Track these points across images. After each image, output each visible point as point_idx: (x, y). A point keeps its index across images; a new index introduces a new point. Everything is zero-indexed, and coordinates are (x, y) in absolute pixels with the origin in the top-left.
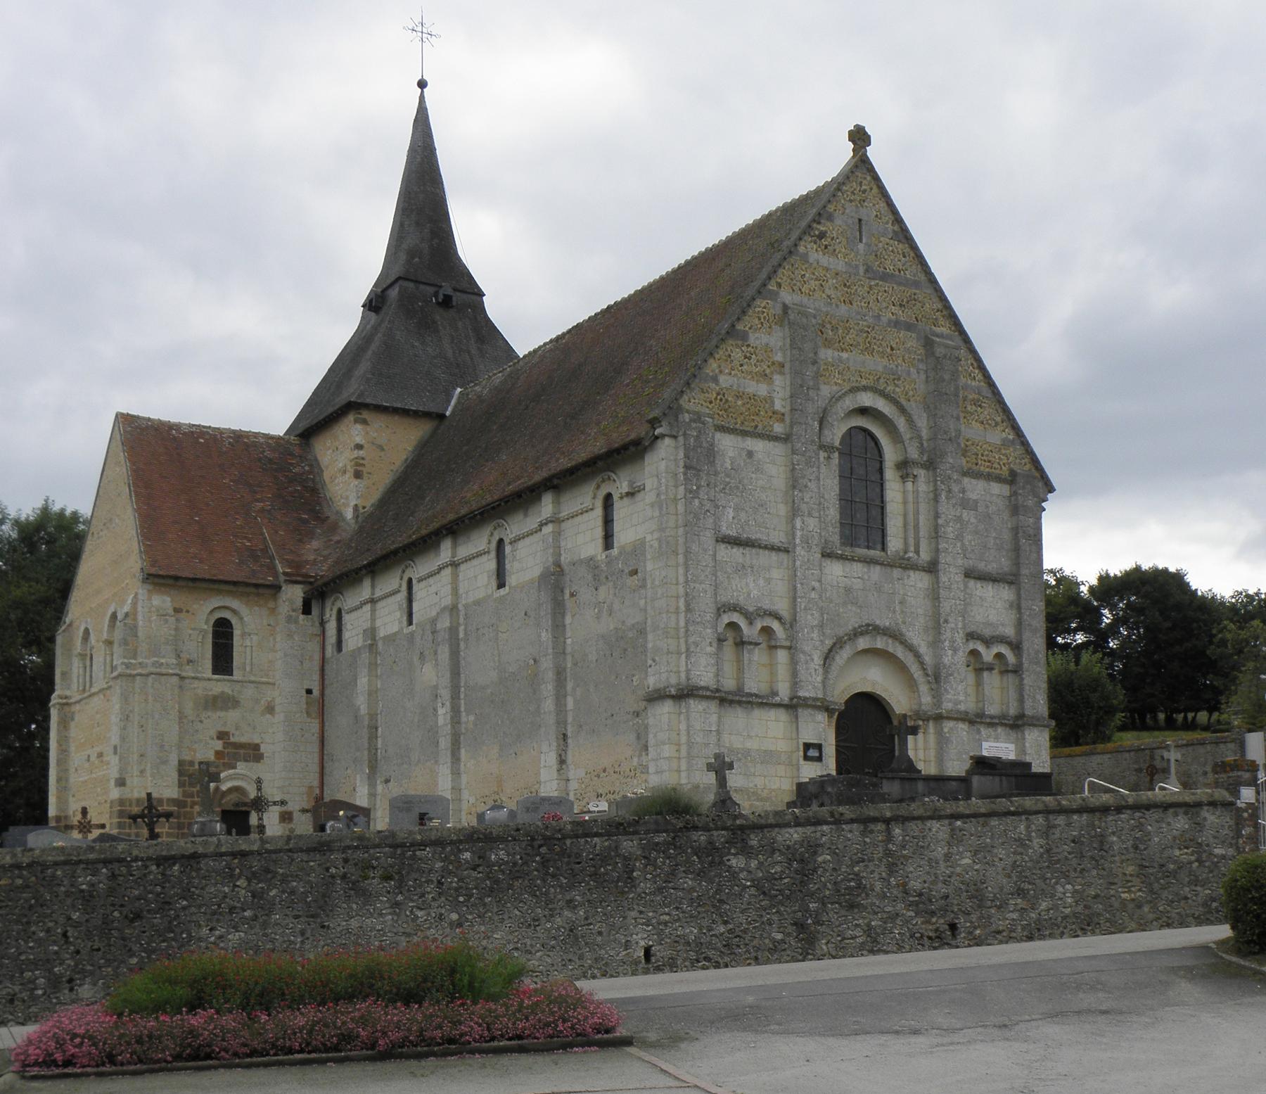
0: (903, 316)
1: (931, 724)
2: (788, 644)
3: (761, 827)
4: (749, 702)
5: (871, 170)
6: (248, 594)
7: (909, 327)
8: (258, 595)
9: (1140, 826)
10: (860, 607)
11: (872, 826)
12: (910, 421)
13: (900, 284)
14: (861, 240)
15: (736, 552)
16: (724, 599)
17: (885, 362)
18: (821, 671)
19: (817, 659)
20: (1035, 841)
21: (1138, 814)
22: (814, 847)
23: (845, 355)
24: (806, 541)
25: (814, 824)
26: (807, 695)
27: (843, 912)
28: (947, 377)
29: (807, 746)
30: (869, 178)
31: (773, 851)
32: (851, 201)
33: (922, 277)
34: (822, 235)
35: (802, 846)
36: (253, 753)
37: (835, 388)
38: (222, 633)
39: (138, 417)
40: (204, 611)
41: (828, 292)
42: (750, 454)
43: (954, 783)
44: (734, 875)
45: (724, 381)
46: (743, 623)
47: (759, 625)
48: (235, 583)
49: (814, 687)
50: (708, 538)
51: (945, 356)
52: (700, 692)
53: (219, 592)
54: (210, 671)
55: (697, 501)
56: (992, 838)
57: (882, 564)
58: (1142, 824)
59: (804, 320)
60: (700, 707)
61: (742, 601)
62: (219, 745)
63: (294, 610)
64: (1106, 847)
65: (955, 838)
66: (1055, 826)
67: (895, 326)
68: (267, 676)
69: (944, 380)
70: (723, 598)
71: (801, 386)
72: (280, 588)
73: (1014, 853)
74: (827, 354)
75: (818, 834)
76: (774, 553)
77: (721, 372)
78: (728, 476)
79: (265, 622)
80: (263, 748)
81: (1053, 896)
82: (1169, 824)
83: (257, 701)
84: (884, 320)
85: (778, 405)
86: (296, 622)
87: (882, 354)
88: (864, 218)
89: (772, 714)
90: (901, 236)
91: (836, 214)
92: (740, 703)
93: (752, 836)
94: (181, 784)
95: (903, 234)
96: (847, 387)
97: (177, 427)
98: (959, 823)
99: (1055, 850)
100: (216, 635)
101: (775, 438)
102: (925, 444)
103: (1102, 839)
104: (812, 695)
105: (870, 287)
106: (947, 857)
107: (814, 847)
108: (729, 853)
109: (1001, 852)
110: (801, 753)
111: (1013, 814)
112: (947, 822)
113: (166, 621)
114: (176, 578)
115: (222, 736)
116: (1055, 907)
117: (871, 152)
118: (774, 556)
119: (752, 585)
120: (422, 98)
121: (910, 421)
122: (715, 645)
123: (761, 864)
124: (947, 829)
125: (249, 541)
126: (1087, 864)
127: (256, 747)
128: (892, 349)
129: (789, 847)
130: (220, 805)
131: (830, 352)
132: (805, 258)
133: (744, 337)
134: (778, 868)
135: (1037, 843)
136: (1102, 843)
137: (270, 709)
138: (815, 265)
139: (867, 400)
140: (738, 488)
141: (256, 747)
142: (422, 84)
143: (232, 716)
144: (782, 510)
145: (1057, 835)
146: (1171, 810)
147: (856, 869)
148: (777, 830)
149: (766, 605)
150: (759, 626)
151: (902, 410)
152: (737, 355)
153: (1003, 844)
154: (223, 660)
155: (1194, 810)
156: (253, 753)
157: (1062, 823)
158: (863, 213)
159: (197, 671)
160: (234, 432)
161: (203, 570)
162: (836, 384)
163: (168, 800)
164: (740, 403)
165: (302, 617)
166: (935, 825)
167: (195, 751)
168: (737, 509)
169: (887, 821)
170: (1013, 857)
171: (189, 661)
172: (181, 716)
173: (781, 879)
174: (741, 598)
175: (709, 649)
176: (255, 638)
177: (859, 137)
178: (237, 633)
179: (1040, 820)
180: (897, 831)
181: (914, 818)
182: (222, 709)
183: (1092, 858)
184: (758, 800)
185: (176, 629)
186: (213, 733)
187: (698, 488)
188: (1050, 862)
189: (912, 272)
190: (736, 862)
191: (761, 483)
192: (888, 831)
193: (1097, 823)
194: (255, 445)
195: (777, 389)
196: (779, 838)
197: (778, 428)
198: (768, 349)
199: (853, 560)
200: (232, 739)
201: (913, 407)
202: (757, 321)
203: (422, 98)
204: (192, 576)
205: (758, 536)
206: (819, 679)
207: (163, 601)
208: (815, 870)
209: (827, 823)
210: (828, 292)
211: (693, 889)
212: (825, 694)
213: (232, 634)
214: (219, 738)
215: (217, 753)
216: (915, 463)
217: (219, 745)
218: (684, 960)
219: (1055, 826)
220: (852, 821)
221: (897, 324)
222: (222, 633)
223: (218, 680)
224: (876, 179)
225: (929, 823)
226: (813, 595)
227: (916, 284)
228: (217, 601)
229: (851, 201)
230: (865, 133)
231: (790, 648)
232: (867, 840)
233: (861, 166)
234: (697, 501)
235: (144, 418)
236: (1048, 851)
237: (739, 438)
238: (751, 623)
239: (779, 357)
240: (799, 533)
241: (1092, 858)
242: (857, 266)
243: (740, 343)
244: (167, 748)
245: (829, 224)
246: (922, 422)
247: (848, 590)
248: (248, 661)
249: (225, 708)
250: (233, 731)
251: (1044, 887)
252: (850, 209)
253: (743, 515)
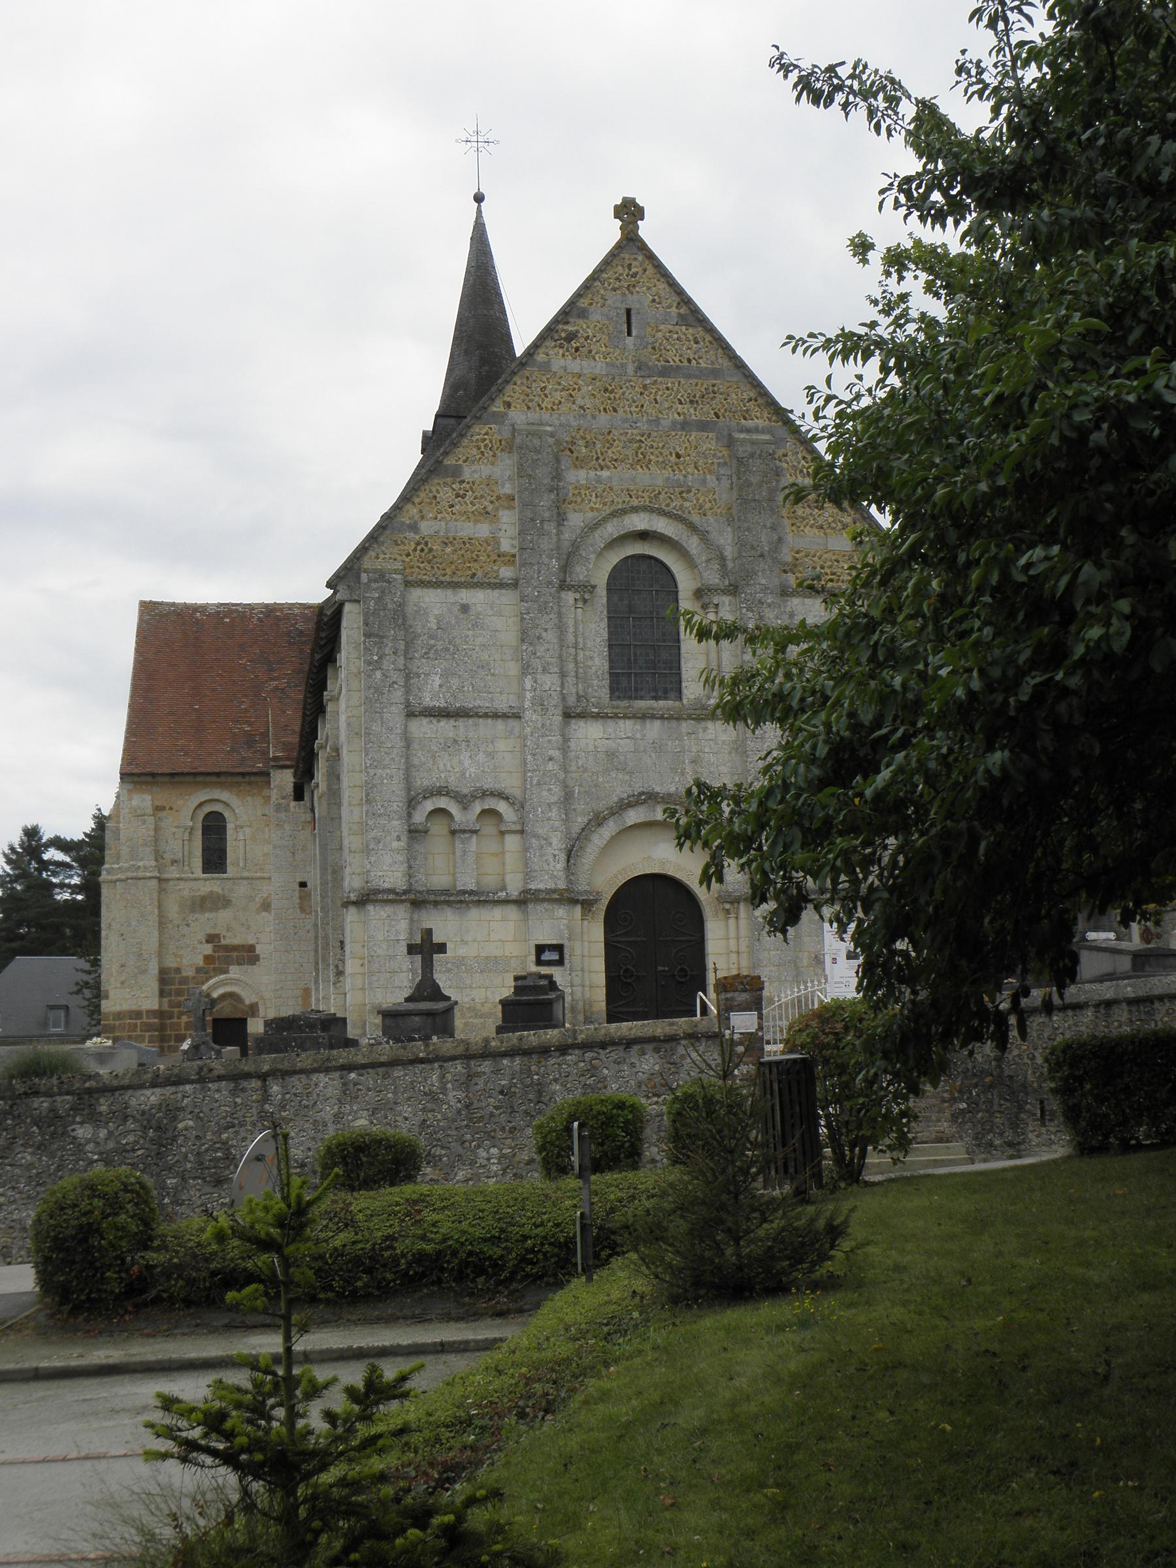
0: (694, 415)
1: (742, 906)
2: (518, 828)
3: (112, 1090)
4: (461, 902)
5: (643, 247)
6: (239, 784)
7: (703, 426)
8: (250, 783)
9: (592, 1070)
10: (631, 773)
11: (244, 1084)
12: (704, 536)
13: (689, 376)
14: (629, 334)
15: (446, 727)
16: (426, 783)
17: (667, 473)
18: (563, 857)
19: (557, 843)
20: (451, 1094)
21: (589, 1055)
22: (172, 1111)
23: (605, 474)
24: (540, 704)
25: (175, 1084)
26: (541, 886)
27: (208, 1189)
28: (754, 480)
29: (540, 949)
30: (640, 258)
31: (125, 1118)
32: (614, 290)
33: (725, 363)
34: (571, 337)
35: (159, 1110)
36: (248, 955)
37: (590, 515)
38: (214, 830)
39: (161, 604)
40: (188, 807)
41: (579, 401)
42: (465, 608)
43: (417, 1019)
44: (79, 1147)
45: (426, 528)
46: (454, 808)
47: (477, 808)
48: (218, 774)
49: (553, 877)
50: (394, 715)
51: (752, 456)
52: (380, 896)
53: (205, 785)
54: (200, 869)
55: (378, 674)
56: (395, 1093)
57: (662, 718)
58: (595, 1068)
59: (536, 442)
60: (383, 914)
61: (453, 782)
62: (208, 949)
63: (283, 798)
64: (545, 1099)
65: (348, 1093)
66: (478, 1075)
67: (683, 429)
68: (262, 870)
69: (750, 485)
70: (422, 780)
71: (532, 520)
72: (269, 774)
73: (424, 1110)
74: (577, 476)
75: (180, 1095)
76: (500, 721)
77: (422, 517)
78: (431, 637)
79: (259, 813)
80: (259, 949)
81: (472, 1163)
82: (633, 1065)
83: (251, 899)
84: (665, 424)
85: (506, 546)
86: (287, 809)
87: (663, 465)
88: (635, 307)
89: (497, 912)
90: (691, 319)
91: (592, 309)
92: (448, 903)
93: (102, 1101)
94: (162, 993)
95: (693, 316)
96: (608, 510)
97: (202, 609)
98: (353, 1075)
99: (476, 1105)
100: (206, 830)
101: (501, 585)
102: (730, 565)
103: (540, 1088)
104: (551, 885)
105: (645, 387)
106: (338, 1117)
107: (172, 1111)
108: (74, 1122)
109: (407, 1110)
110: (533, 958)
111: (422, 1061)
112: (337, 1074)
113: (144, 822)
114: (153, 775)
115: (211, 939)
116: (476, 1177)
117: (646, 230)
118: (500, 725)
119: (467, 762)
120: (479, 211)
121: (704, 536)
122: (404, 838)
123: (110, 1133)
124: (337, 1083)
125: (250, 724)
126: (519, 1120)
127: (251, 948)
128: (678, 456)
129: (143, 1113)
130: (211, 1014)
131: (582, 474)
132: (546, 367)
133: (456, 472)
134: (131, 1138)
135: (454, 1096)
136: (540, 1093)
137: (266, 906)
138: (562, 372)
139: (639, 522)
140: (447, 650)
141: (251, 948)
142: (479, 198)
143: (224, 916)
144: (513, 668)
145: (481, 1086)
146: (636, 1048)
147: (224, 1136)
148: (130, 1092)
149: (488, 784)
150: (478, 810)
151: (693, 528)
152: (446, 495)
153: (409, 1099)
154: (215, 859)
155: (668, 1046)
156: (248, 955)
157: (487, 1070)
158: (632, 301)
159: (183, 871)
160: (267, 606)
161: (184, 763)
162: (592, 509)
163: (148, 1011)
164: (448, 550)
165: (293, 804)
166: (323, 1079)
167: (181, 957)
168: (446, 675)
169: (263, 1077)
170: (421, 1116)
171: (174, 862)
172: (162, 922)
173: (134, 1150)
174: (452, 779)
175: (395, 844)
176: (248, 830)
177: (629, 212)
178: (230, 826)
179: (459, 1067)
180: (275, 1088)
181: (295, 1072)
182: (211, 910)
183: (527, 1113)
184: (476, 1016)
185: (156, 829)
186: (202, 936)
187: (380, 658)
188: (470, 1120)
189: (709, 359)
190: (83, 1132)
191: (480, 640)
192: (265, 1089)
193: (533, 1068)
194: (287, 617)
195: (504, 527)
196: (133, 1102)
197: (506, 573)
198: (490, 482)
199: (616, 717)
200: (223, 942)
201: (711, 523)
202: (475, 451)
203: (479, 211)
204: (170, 771)
205: (478, 703)
206: (561, 865)
207: (144, 800)
208: (174, 1138)
209: (191, 1082)
210: (579, 401)
211: (30, 1166)
212: (570, 882)
213: (224, 828)
214: (208, 942)
215: (207, 958)
216: (725, 592)
217: (208, 949)
218: (20, 1249)
219: (478, 1075)
220: (220, 1078)
221: (685, 426)
222: (214, 830)
223: (206, 880)
224: (651, 256)
225: (314, 1077)
226: (550, 766)
227: (715, 373)
228: (203, 795)
229: (614, 290)
230: (636, 205)
231: (522, 832)
232: (238, 1100)
233: (631, 241)
234: (378, 674)
235: (167, 604)
236: (468, 1107)
237: (449, 592)
238: (465, 808)
239: (507, 489)
240: (528, 695)
241: (527, 1113)
242: (623, 366)
243: (449, 480)
244: (145, 956)
245: (581, 321)
246: (726, 539)
247: (611, 755)
248: (241, 856)
249: (215, 909)
250: (224, 933)
251: (460, 1151)
252: (613, 299)
253: (455, 682)
